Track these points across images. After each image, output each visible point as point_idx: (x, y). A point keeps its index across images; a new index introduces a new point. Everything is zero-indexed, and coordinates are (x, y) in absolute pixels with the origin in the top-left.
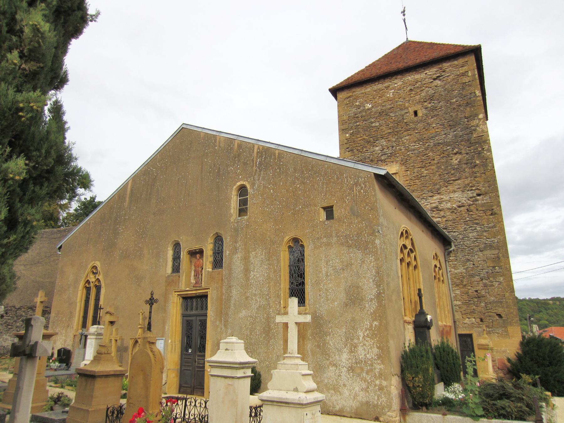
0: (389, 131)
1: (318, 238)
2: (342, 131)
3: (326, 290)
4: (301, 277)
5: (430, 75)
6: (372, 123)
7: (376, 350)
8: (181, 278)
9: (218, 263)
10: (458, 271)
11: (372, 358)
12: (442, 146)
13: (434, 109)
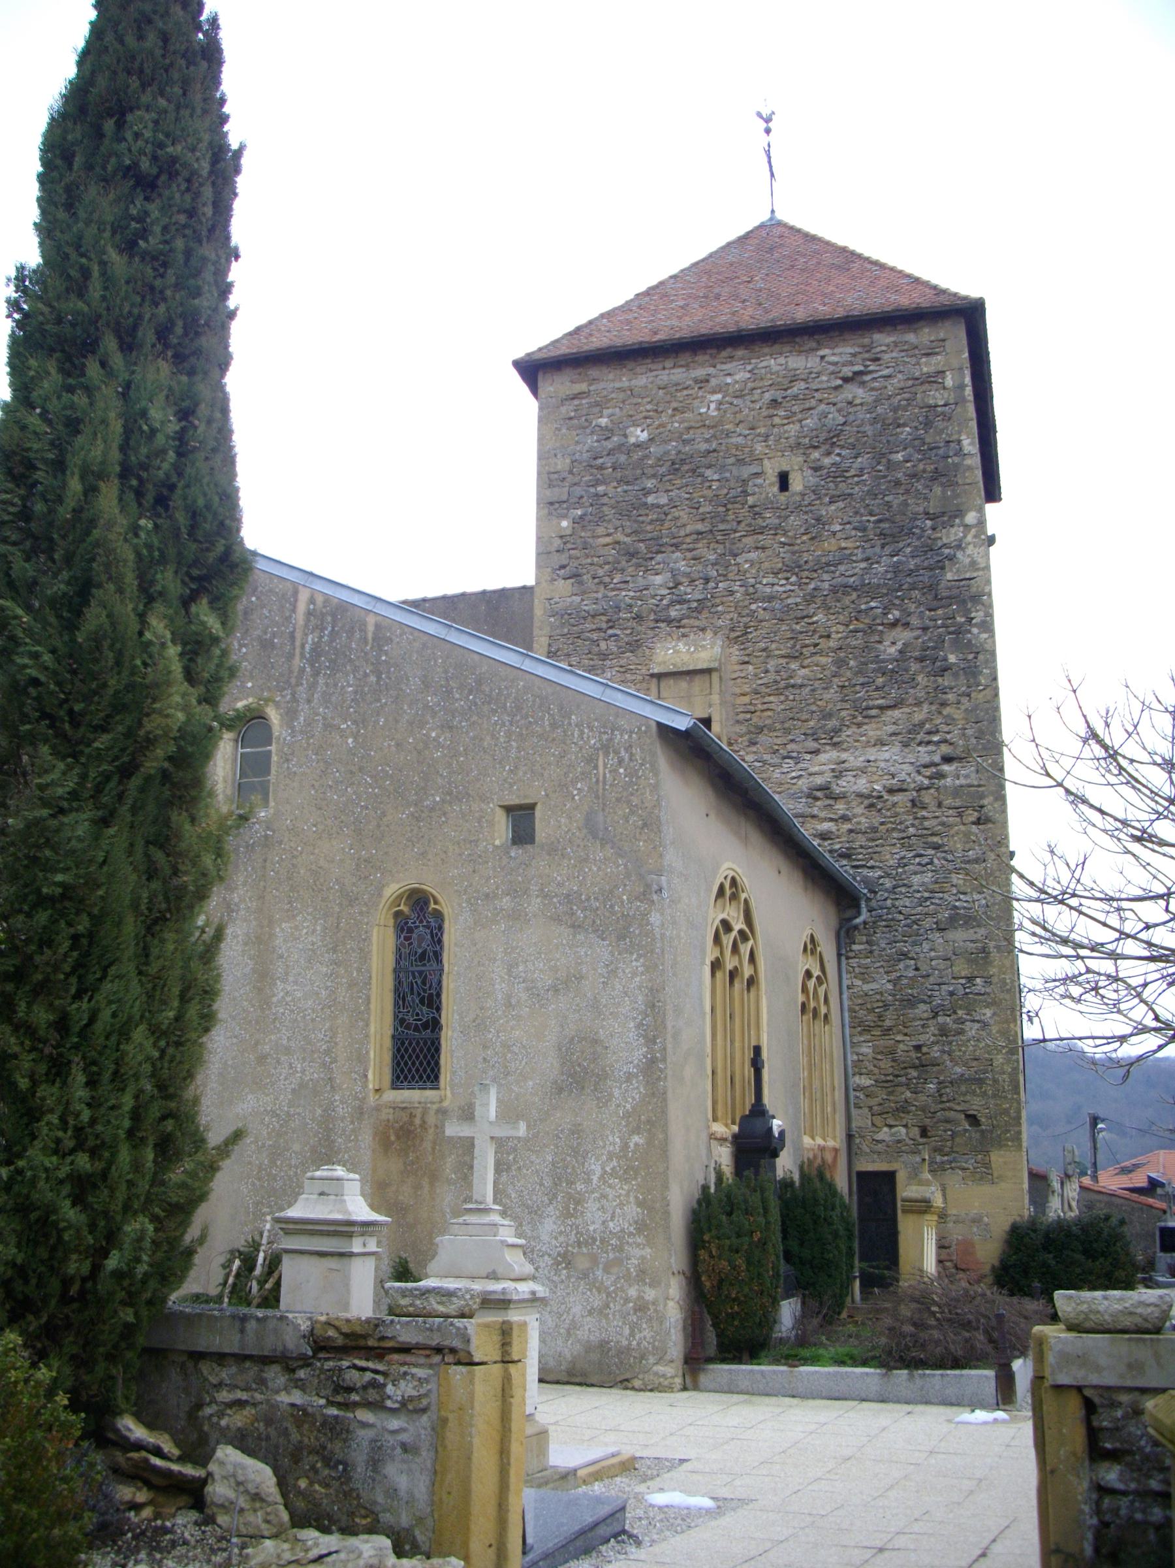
0: (700, 527)
1: (487, 896)
2: (549, 507)
3: (507, 1046)
4: (430, 1006)
6: (647, 492)
7: (633, 1211)
10: (874, 986)
11: (623, 1230)
12: (854, 595)
13: (838, 474)
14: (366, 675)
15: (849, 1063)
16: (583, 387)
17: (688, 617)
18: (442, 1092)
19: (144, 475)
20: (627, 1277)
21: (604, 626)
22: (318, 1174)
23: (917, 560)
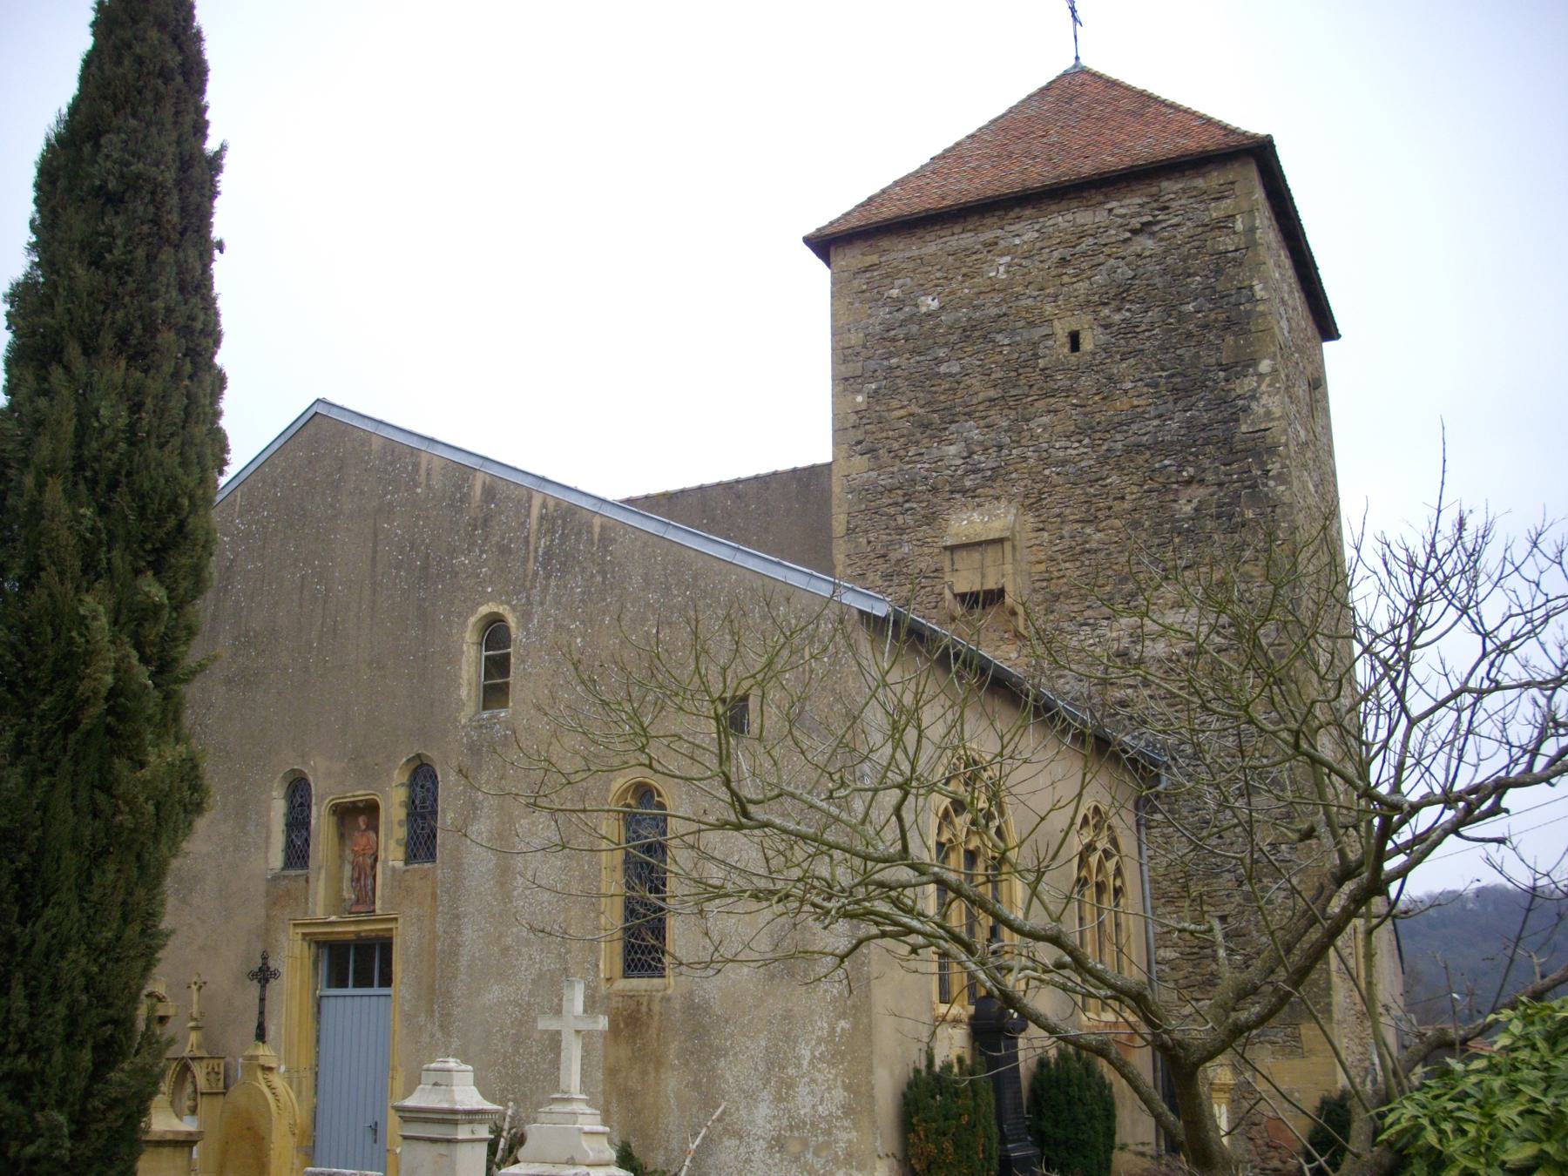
0: (992, 393)
2: (844, 382)
5: (1123, 216)
6: (939, 361)
7: (839, 1094)
8: (312, 885)
9: (421, 845)
11: (831, 1114)
13: (1130, 329)
14: (593, 576)
15: (1151, 935)
16: (874, 259)
17: (983, 487)
18: (666, 981)
19: (96, 466)
20: (835, 1160)
21: (901, 500)
22: (433, 1065)
23: (1211, 414)
